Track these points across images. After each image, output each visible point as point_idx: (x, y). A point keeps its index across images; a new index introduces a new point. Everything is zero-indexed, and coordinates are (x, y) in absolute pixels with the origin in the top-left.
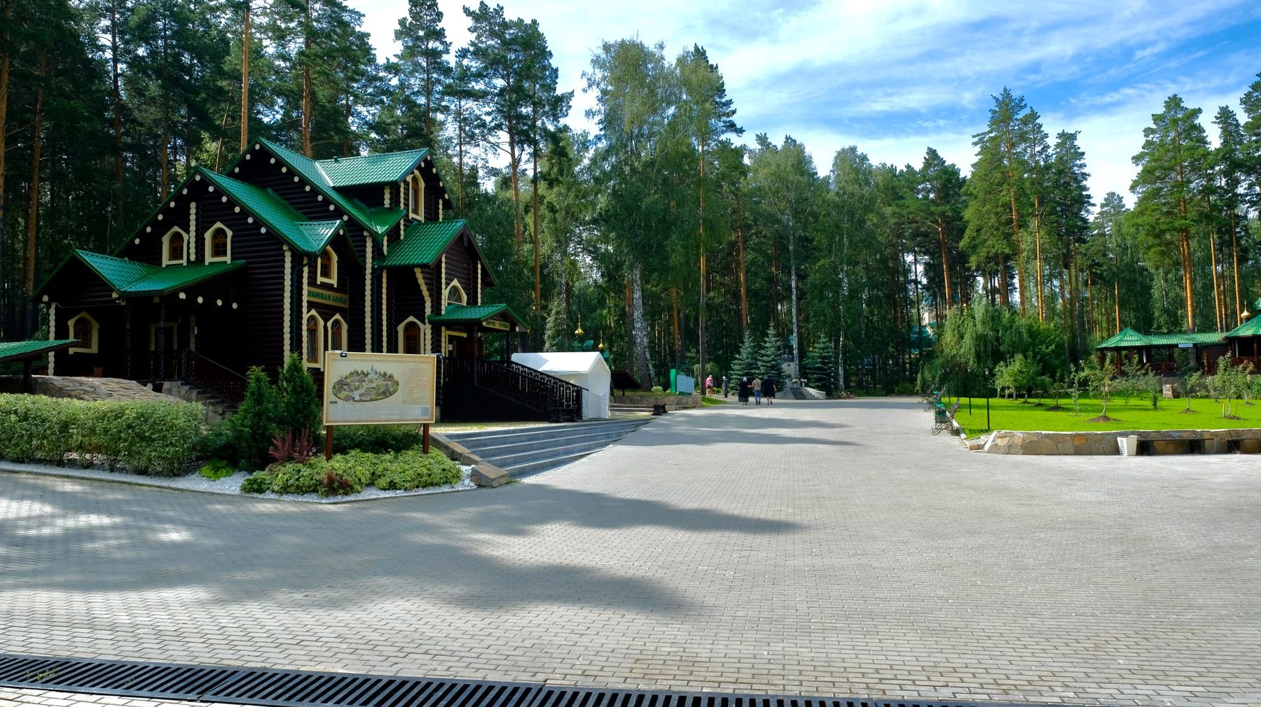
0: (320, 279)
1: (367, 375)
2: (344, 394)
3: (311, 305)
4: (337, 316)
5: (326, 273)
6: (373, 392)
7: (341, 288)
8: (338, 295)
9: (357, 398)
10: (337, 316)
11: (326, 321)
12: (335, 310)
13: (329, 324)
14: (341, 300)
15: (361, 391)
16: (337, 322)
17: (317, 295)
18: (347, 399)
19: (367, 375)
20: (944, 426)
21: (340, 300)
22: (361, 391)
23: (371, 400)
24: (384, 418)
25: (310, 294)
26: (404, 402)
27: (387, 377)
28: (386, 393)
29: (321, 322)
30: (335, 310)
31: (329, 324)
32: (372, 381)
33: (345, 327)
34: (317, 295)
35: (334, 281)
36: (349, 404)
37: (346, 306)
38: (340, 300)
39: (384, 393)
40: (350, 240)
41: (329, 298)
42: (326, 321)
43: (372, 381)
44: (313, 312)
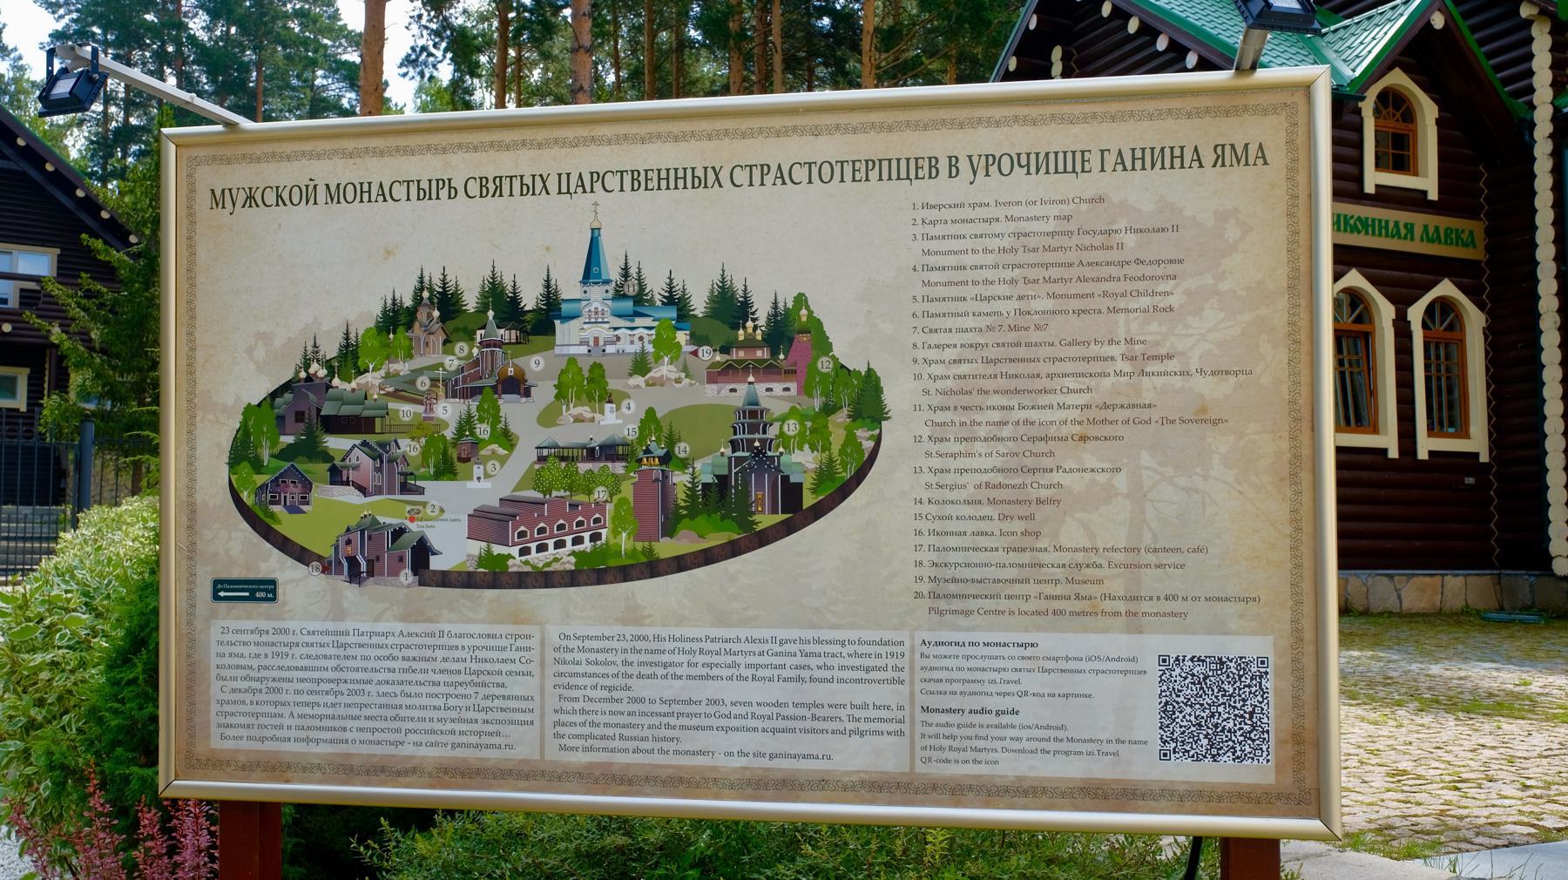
0: (1373, 178)
1: (542, 321)
2: (332, 510)
3: (1345, 257)
4: (1446, 288)
5: (1398, 154)
6: (613, 495)
7: (1454, 198)
8: (1443, 222)
9: (454, 548)
10: (1446, 288)
11: (1402, 304)
12: (1437, 268)
13: (1416, 313)
14: (1463, 238)
15: (488, 485)
16: (1443, 308)
17: (1365, 225)
18: (363, 558)
19: (542, 321)
20: (483, 430)
21: (1450, 237)
22: (488, 485)
23: (595, 571)
24: (727, 750)
25: (1339, 223)
26: (945, 594)
27: (752, 335)
28: (753, 502)
29: (1385, 311)
30: (1437, 268)
31: (1416, 313)
32: (590, 384)
33: (1475, 321)
34: (1365, 225)
35: (1428, 181)
36: (380, 611)
37: (1476, 253)
38: (1450, 237)
39: (719, 496)
40: (1471, 39)
41: (1415, 234)
42: (1402, 304)
43: (590, 384)
44: (1354, 279)
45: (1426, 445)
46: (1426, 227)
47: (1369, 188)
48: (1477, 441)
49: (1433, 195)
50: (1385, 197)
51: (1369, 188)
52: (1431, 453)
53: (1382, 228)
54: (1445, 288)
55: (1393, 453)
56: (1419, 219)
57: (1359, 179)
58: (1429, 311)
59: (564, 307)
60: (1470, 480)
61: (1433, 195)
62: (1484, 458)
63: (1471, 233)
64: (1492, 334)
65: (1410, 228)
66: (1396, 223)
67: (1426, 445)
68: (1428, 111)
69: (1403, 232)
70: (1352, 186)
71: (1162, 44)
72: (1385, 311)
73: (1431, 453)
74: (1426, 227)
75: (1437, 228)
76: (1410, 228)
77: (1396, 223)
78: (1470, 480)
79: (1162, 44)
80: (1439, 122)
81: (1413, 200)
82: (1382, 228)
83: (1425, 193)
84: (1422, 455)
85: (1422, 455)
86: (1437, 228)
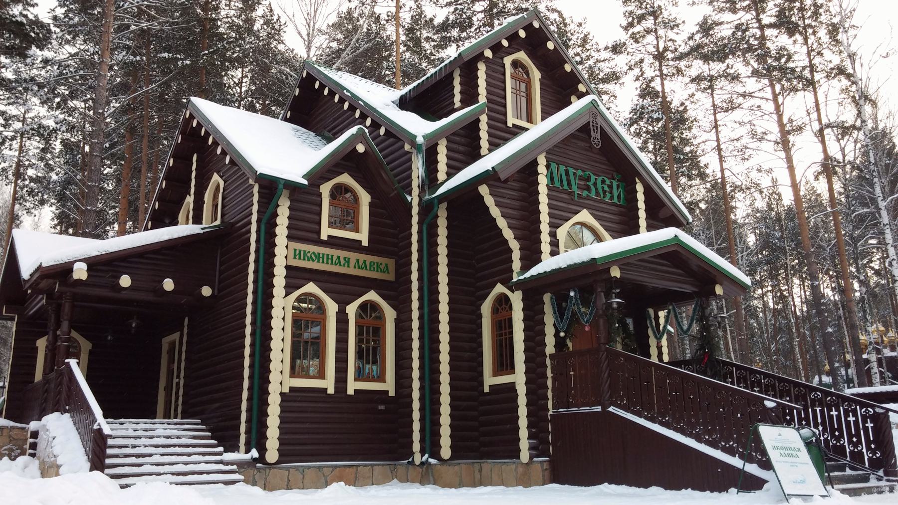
5: (348, 219)
8: (369, 258)
11: (342, 304)
12: (368, 284)
13: (352, 309)
14: (378, 267)
17: (306, 256)
29: (332, 307)
30: (368, 284)
31: (352, 309)
35: (363, 237)
41: (350, 264)
45: (352, 386)
46: (358, 260)
47: (324, 237)
48: (389, 386)
49: (365, 243)
50: (333, 242)
51: (324, 237)
52: (356, 391)
53: (329, 259)
54: (372, 296)
55: (331, 391)
56: (353, 256)
57: (319, 233)
58: (363, 307)
59: (110, 442)
60: (382, 407)
61: (365, 243)
62: (392, 393)
63: (387, 265)
64: (398, 321)
65: (347, 261)
66: (339, 257)
67: (352, 386)
68: (365, 198)
69: (343, 262)
70: (315, 236)
71: (357, 114)
72: (332, 307)
73: (356, 391)
74: (358, 260)
75: (365, 261)
76: (347, 261)
77: (339, 257)
78: (382, 407)
79: (357, 114)
80: (370, 204)
81: (354, 246)
82: (329, 259)
83: (361, 242)
84: (350, 392)
85: (350, 392)
86: (365, 261)
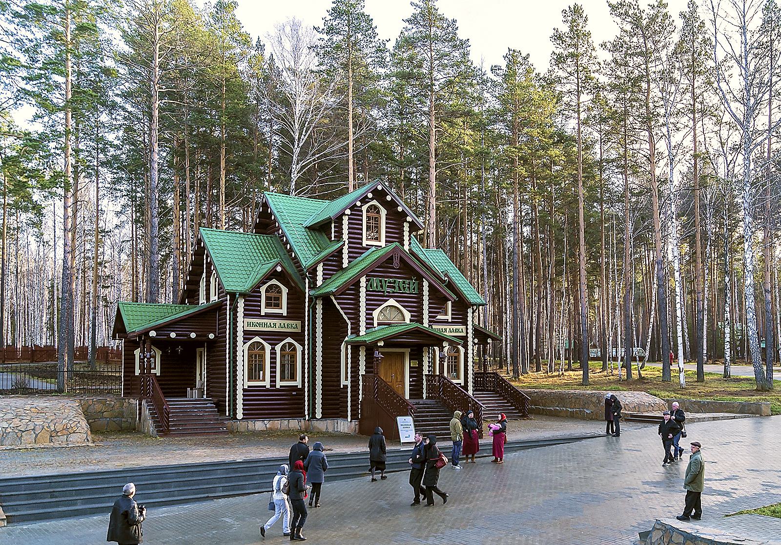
11: (273, 345)
13: (278, 348)
31: (278, 348)
42: (273, 345)
55: (268, 386)
72: (268, 348)
85: (278, 386)
